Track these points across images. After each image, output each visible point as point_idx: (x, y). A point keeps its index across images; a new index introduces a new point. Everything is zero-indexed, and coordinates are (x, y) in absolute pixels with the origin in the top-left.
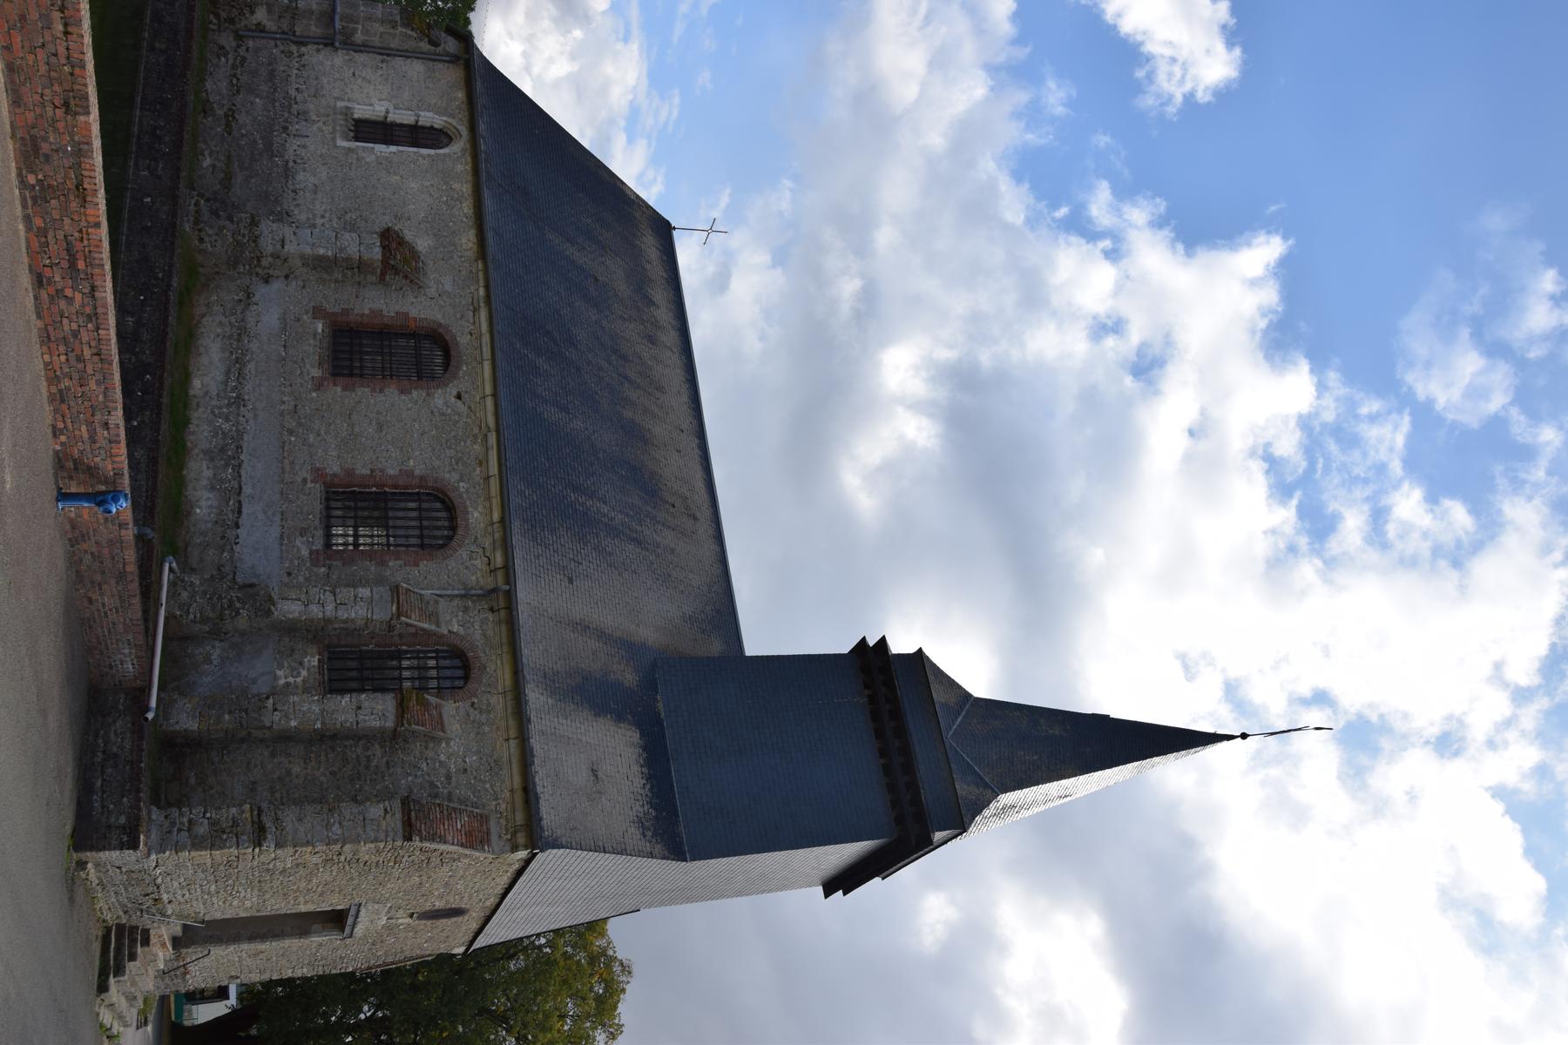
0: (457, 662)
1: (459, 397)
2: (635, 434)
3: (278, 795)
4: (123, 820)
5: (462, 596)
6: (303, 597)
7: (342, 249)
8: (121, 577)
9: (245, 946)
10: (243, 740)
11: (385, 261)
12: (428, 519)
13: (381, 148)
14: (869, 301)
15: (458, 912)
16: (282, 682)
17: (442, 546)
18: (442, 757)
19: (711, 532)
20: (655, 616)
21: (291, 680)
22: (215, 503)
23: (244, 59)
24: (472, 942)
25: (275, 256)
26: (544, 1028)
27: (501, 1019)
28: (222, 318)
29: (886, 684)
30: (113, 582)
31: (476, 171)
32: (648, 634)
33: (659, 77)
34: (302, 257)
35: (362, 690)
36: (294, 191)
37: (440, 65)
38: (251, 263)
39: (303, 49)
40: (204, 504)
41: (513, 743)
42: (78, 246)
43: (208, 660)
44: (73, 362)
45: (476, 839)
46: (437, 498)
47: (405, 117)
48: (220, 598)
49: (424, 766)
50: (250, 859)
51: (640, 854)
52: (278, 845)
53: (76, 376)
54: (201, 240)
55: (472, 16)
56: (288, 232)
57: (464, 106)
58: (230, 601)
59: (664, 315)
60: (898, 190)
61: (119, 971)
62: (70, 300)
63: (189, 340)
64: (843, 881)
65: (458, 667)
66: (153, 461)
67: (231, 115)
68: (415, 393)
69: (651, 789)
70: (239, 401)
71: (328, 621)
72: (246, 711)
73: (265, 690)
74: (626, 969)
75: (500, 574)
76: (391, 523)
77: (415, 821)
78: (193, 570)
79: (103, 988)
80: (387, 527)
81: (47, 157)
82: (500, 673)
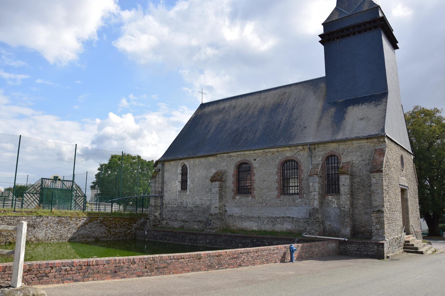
0: (330, 158)
1: (255, 160)
2: (262, 111)
3: (368, 207)
4: (376, 247)
5: (311, 157)
6: (313, 200)
7: (217, 192)
8: (311, 247)
9: (410, 216)
10: (353, 216)
11: (219, 181)
12: (289, 167)
13: (188, 183)
14: (214, 45)
15: (402, 157)
16: (336, 206)
17: (297, 163)
18: (358, 162)
19: (288, 88)
20: (314, 104)
21: (336, 203)
22: (287, 223)
23: (168, 218)
24: (410, 153)
25: (220, 209)
26: (434, 132)
27: (431, 144)
28: (237, 222)
29: (333, 34)
30: (312, 249)
31: (193, 158)
32: (320, 105)
33: (154, 109)
34: (219, 202)
35: (339, 184)
36: (202, 205)
37: (165, 168)
38: (222, 215)
39: (164, 203)
40: (287, 226)
41: (353, 142)
42: (231, 256)
43: (330, 225)
44: (259, 258)
45: (382, 152)
46: (284, 165)
47: (180, 177)
48: (313, 222)
49: (360, 167)
50: (387, 214)
51: (386, 105)
52: (383, 207)
53: (262, 257)
54: (217, 228)
55: (147, 161)
56: (213, 206)
57: (175, 162)
58: (314, 219)
59: (227, 104)
60: (181, 40)
61: (417, 248)
62: (244, 259)
63: (243, 230)
64: (394, 44)
65: (331, 158)
66: (277, 239)
67: (183, 221)
68: (255, 172)
69: (365, 102)
70: (259, 218)
71: (319, 194)
72: (345, 215)
73: (339, 210)
74: (416, 108)
75: (305, 147)
76: (288, 177)
77: (376, 168)
78: (305, 229)
79: (422, 253)
80: (290, 178)
81: (211, 263)
82: (333, 147)
